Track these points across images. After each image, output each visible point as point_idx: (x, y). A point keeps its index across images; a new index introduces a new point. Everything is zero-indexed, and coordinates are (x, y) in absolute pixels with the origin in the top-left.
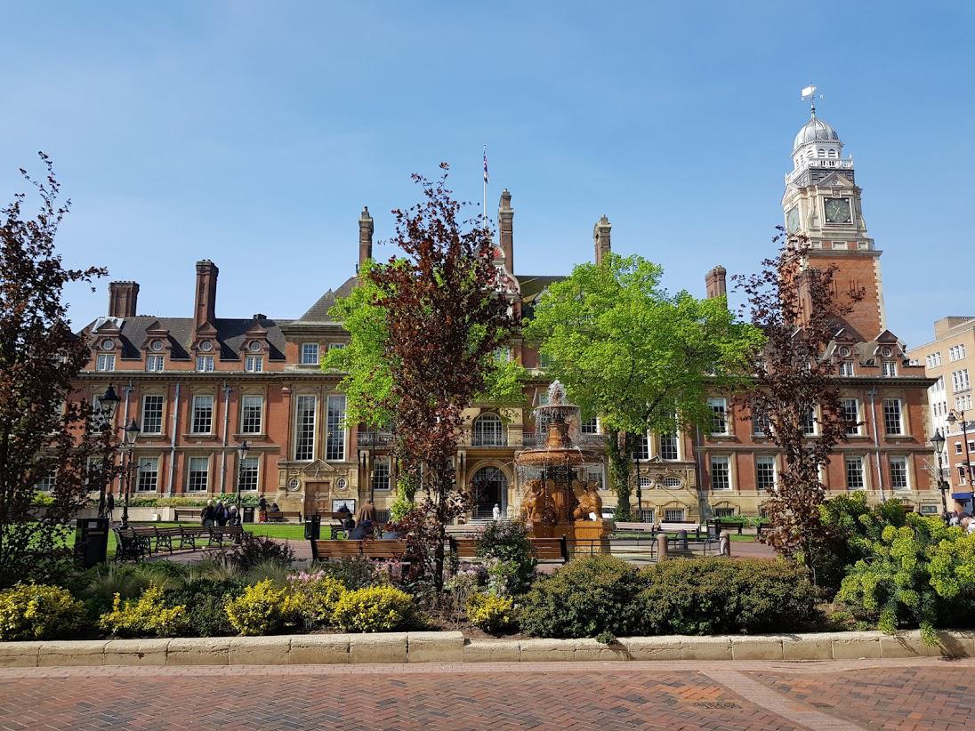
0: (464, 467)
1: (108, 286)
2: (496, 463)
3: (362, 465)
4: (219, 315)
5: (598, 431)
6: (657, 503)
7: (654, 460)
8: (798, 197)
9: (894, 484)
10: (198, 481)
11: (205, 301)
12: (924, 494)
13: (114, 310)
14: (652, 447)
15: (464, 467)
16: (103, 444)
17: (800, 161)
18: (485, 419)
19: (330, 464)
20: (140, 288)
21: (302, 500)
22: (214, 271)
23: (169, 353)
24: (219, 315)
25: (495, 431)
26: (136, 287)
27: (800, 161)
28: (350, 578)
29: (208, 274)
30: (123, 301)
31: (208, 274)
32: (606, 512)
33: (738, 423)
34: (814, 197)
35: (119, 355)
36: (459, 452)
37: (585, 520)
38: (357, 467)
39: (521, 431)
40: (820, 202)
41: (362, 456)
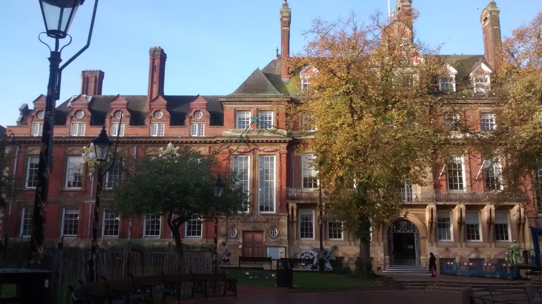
1: (80, 74)
3: (290, 217)
4: (168, 91)
9: (498, 238)
10: (194, 227)
11: (156, 79)
13: (85, 90)
16: (489, 80)
19: (263, 215)
20: (105, 75)
21: (240, 246)
22: (163, 57)
23: (128, 120)
24: (168, 91)
26: (101, 75)
29: (158, 61)
30: (92, 85)
31: (158, 61)
35: (89, 123)
37: (240, 257)
38: (286, 217)
41: (290, 208)
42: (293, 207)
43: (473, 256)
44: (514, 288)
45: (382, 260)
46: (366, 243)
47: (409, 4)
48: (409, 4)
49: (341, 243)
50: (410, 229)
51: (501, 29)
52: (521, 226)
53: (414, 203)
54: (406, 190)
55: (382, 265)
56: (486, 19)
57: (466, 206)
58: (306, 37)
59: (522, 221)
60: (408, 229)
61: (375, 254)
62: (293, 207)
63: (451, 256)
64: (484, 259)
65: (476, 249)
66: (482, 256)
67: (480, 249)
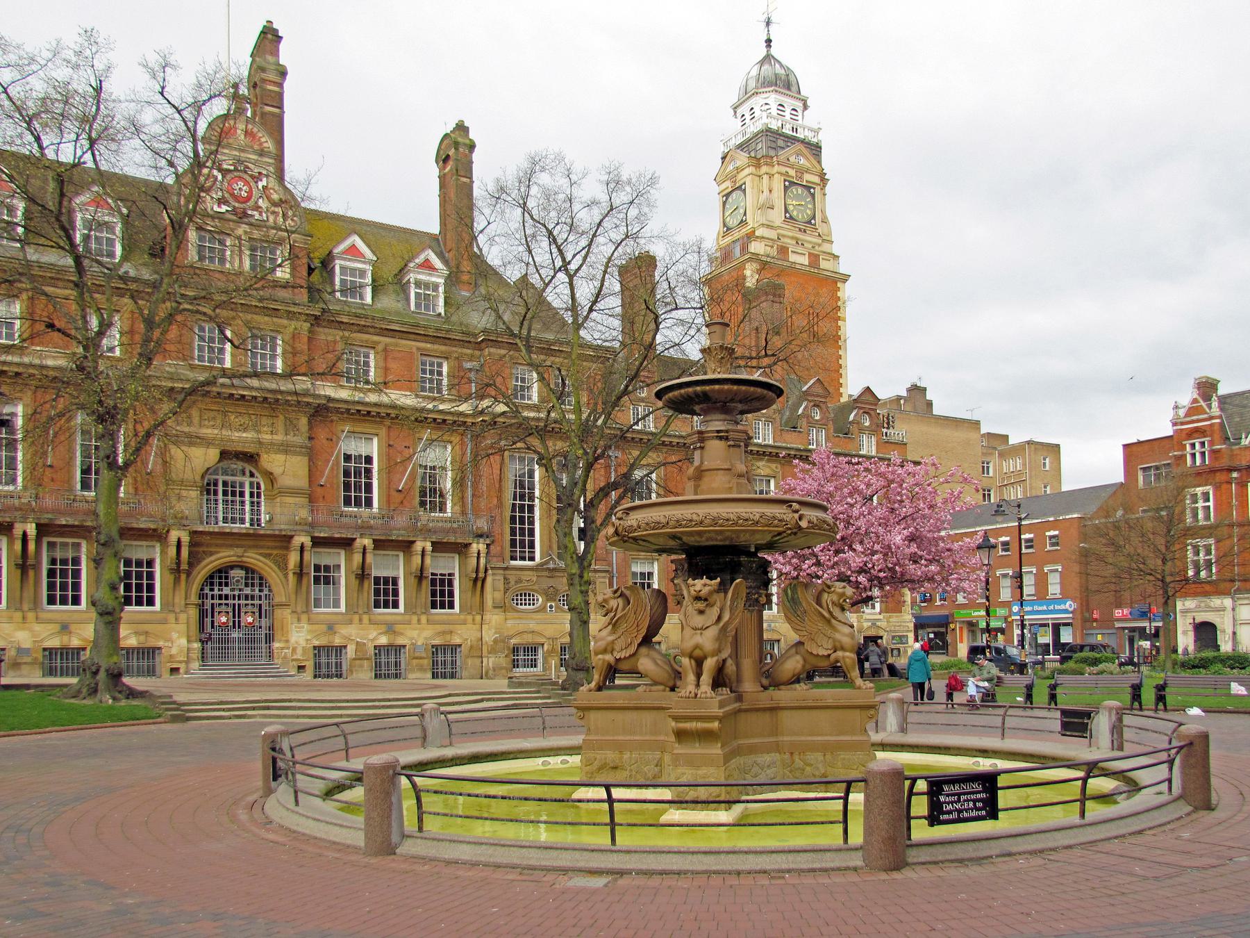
0: (184, 566)
2: (254, 558)
5: (449, 510)
6: (548, 634)
7: (542, 564)
8: (747, 171)
12: (895, 618)
14: (541, 541)
15: (184, 566)
17: (748, 117)
18: (225, 473)
25: (220, 496)
27: (748, 117)
28: (237, 625)
32: (390, 835)
33: (1129, 749)
34: (771, 176)
36: (174, 535)
39: (304, 501)
40: (778, 184)
42: (179, 541)
43: (383, 640)
44: (383, 707)
45: (181, 651)
46: (581, 620)
47: (278, 79)
48: (278, 79)
49: (76, 616)
50: (253, 585)
51: (286, 116)
52: (479, 584)
53: (262, 532)
54: (247, 503)
55: (180, 662)
56: (448, 157)
57: (375, 541)
58: (722, 315)
59: (481, 575)
60: (247, 585)
61: (167, 640)
62: (179, 541)
63: (338, 641)
64: (404, 646)
65: (390, 629)
66: (400, 641)
67: (398, 628)
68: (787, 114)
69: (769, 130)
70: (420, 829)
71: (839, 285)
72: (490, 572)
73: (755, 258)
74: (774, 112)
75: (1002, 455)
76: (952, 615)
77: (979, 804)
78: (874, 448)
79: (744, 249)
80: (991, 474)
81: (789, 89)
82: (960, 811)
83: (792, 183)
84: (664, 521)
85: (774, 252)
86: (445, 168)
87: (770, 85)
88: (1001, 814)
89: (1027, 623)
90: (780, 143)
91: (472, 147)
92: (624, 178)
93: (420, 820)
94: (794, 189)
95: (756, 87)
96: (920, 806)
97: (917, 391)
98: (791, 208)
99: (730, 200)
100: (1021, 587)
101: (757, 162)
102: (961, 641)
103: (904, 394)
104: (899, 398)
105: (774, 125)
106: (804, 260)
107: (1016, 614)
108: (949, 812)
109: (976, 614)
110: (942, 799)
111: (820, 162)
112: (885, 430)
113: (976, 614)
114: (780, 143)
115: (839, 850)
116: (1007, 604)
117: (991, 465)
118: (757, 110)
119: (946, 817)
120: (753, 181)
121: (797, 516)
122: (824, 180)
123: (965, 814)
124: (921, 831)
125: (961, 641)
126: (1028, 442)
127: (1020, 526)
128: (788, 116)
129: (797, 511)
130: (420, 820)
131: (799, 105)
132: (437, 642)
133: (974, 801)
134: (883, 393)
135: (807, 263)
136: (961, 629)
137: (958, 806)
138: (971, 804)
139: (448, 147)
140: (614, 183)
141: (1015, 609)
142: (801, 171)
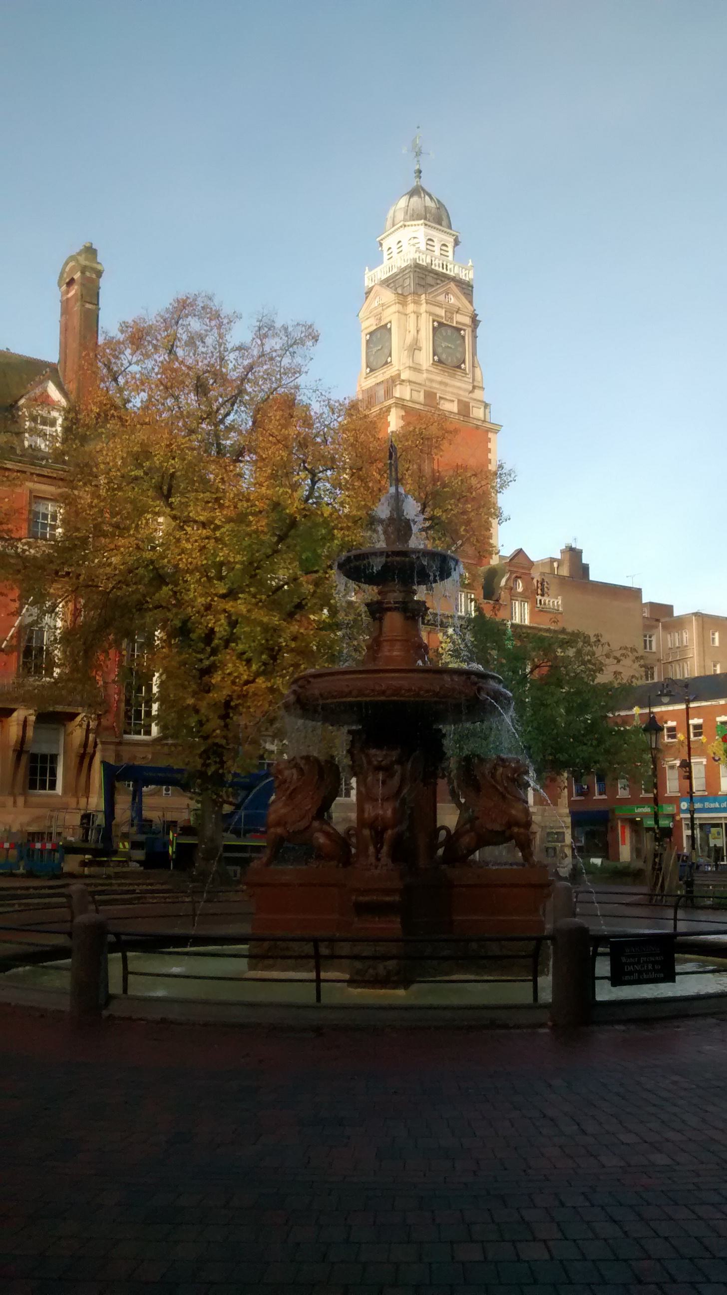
17: (395, 250)
27: (395, 250)
59: (90, 750)
68: (437, 249)
69: (417, 266)
70: (125, 990)
71: (490, 435)
72: (99, 746)
73: (400, 404)
74: (423, 247)
75: (666, 627)
76: (613, 811)
77: (657, 967)
78: (527, 617)
79: (388, 393)
80: (654, 649)
81: (441, 224)
82: (640, 973)
83: (441, 324)
84: (346, 690)
85: (421, 397)
86: (68, 292)
87: (419, 218)
88: (677, 978)
89: (697, 822)
90: (430, 280)
91: (99, 274)
92: (278, 325)
93: (125, 980)
94: (443, 330)
95: (405, 220)
96: (603, 967)
97: (574, 554)
98: (439, 350)
99: (374, 338)
100: (689, 778)
101: (402, 299)
102: (624, 843)
103: (558, 556)
104: (552, 560)
105: (424, 261)
106: (454, 407)
107: (685, 811)
108: (630, 973)
109: (640, 810)
110: (624, 960)
111: (471, 302)
112: (539, 597)
113: (640, 810)
114: (430, 280)
115: (528, 1007)
116: (674, 800)
117: (654, 639)
118: (404, 243)
119: (627, 978)
120: (399, 320)
121: (475, 688)
122: (475, 322)
123: (645, 976)
124: (605, 992)
125: (624, 843)
126: (697, 614)
127: (688, 708)
128: (437, 252)
129: (475, 684)
130: (125, 980)
131: (450, 241)
132: (33, 829)
133: (653, 963)
134: (534, 555)
135: (455, 410)
136: (623, 827)
137: (637, 968)
138: (650, 967)
139: (73, 270)
140: (264, 330)
141: (684, 805)
142: (453, 311)
